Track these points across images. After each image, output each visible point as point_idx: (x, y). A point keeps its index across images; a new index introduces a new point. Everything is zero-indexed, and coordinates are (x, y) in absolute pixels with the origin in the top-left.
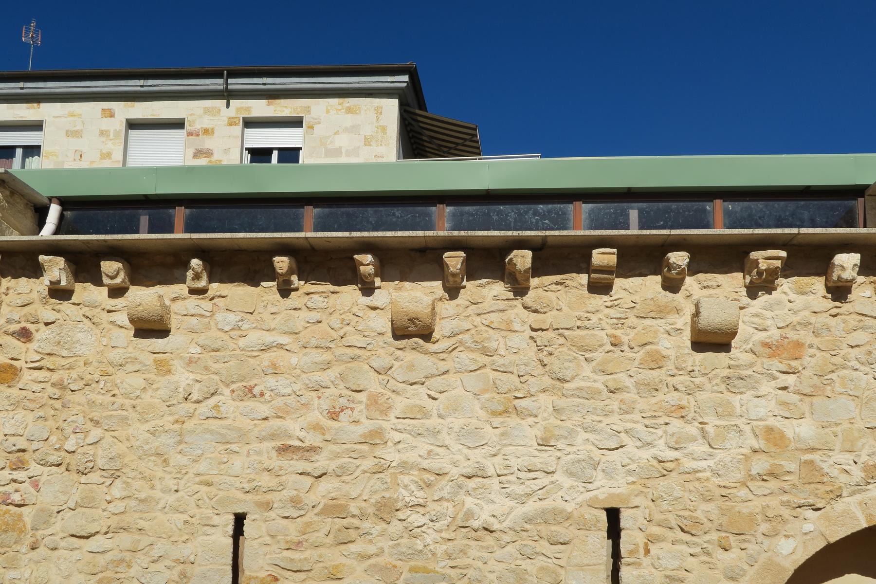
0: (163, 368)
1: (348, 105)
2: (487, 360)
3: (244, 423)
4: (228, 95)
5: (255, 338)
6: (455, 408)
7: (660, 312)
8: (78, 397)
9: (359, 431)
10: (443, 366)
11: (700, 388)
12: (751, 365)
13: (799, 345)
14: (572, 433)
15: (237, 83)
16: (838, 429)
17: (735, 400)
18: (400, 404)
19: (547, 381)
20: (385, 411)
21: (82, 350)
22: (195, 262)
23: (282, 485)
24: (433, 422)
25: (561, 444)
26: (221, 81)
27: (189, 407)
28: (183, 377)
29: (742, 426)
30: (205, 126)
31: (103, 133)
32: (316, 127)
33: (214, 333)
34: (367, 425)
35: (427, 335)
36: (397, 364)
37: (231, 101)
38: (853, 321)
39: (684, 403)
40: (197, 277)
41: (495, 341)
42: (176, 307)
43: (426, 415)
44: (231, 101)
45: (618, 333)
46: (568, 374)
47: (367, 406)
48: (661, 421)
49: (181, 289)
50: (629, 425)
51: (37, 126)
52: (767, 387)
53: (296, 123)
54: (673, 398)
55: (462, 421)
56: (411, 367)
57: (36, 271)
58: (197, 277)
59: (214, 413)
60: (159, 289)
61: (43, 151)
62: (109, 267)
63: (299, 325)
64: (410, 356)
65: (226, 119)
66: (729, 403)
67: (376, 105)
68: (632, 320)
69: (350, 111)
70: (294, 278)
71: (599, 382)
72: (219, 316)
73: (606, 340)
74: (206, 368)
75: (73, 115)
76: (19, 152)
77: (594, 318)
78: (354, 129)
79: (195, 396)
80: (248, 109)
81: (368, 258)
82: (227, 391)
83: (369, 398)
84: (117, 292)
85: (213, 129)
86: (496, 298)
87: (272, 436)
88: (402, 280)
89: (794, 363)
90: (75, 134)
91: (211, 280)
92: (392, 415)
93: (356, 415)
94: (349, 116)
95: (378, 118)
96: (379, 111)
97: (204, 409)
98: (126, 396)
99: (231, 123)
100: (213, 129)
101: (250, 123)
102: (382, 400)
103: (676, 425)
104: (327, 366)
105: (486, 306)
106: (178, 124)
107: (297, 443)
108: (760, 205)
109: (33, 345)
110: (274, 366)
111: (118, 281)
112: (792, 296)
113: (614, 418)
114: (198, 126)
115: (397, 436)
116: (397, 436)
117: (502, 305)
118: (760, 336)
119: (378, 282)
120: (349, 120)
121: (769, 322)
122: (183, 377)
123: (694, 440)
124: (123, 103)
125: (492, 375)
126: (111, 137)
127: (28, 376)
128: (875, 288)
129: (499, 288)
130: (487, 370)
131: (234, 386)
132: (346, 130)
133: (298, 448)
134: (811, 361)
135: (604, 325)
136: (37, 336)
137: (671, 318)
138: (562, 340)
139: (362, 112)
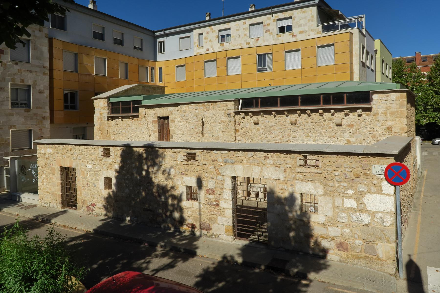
0: (259, 129)
2: (305, 128)
3: (270, 138)
4: (273, 13)
5: (271, 124)
6: (300, 136)
7: (331, 119)
8: (247, 134)
9: (287, 139)
10: (298, 129)
11: (337, 133)
12: (345, 129)
13: (353, 125)
14: (318, 140)
15: (274, 10)
16: (359, 140)
17: (343, 135)
18: (292, 135)
19: (314, 131)
20: (290, 136)
21: (247, 127)
22: (262, 113)
24: (297, 138)
25: (316, 142)
26: (270, 10)
27: (263, 136)
28: (261, 131)
29: (344, 139)
30: (268, 23)
31: (244, 29)
33: (265, 124)
34: (288, 139)
35: (296, 124)
36: (292, 128)
38: (362, 120)
39: (335, 135)
40: (262, 115)
41: (306, 124)
42: (260, 119)
43: (296, 137)
45: (325, 123)
46: (317, 130)
47: (288, 135)
48: (331, 138)
49: (260, 116)
50: (326, 139)
51: (229, 29)
52: (348, 132)
53: (290, 18)
54: (333, 134)
55: (301, 138)
56: (294, 129)
57: (240, 115)
58: (262, 115)
59: (266, 137)
60: (257, 116)
61: (231, 35)
62: (250, 114)
63: (277, 122)
64: (294, 127)
65: (272, 20)
66: (341, 135)
67: (310, 9)
68: (327, 121)
69: (304, 12)
70: (276, 115)
71: (322, 131)
72: (266, 121)
73: (323, 124)
74: (264, 129)
75: (237, 25)
76: (226, 36)
77: (321, 120)
78: (305, 18)
79: (263, 134)
80: (278, 16)
81: (286, 112)
82: (268, 133)
83: (288, 134)
84: (251, 117)
85: (270, 23)
86: (306, 117)
87: (274, 141)
88: (292, 114)
89: (352, 128)
90: (238, 30)
91: (264, 115)
92: (291, 137)
93: (286, 137)
94: (304, 14)
95: (311, 13)
96: (311, 11)
97: (265, 136)
98: (254, 134)
99: (274, 21)
100: (270, 23)
101: (278, 20)
102: (290, 135)
103: (334, 139)
104: (281, 129)
105: (304, 118)
106: (261, 23)
107: (278, 142)
109: (241, 126)
110: (274, 129)
111: (251, 116)
112: (352, 116)
113: (324, 138)
114: (266, 23)
115: (292, 141)
116: (292, 141)
117: (307, 118)
118: (347, 123)
119: (288, 115)
120: (303, 15)
121: (348, 121)
122: (261, 131)
123: (336, 141)
124: (248, 20)
125: (306, 130)
127: (240, 131)
128: (437, 65)
129: (306, 115)
130: (305, 129)
131: (269, 132)
133: (278, 142)
134: (355, 128)
135: (322, 122)
136: (241, 124)
137: (333, 121)
138: (316, 124)
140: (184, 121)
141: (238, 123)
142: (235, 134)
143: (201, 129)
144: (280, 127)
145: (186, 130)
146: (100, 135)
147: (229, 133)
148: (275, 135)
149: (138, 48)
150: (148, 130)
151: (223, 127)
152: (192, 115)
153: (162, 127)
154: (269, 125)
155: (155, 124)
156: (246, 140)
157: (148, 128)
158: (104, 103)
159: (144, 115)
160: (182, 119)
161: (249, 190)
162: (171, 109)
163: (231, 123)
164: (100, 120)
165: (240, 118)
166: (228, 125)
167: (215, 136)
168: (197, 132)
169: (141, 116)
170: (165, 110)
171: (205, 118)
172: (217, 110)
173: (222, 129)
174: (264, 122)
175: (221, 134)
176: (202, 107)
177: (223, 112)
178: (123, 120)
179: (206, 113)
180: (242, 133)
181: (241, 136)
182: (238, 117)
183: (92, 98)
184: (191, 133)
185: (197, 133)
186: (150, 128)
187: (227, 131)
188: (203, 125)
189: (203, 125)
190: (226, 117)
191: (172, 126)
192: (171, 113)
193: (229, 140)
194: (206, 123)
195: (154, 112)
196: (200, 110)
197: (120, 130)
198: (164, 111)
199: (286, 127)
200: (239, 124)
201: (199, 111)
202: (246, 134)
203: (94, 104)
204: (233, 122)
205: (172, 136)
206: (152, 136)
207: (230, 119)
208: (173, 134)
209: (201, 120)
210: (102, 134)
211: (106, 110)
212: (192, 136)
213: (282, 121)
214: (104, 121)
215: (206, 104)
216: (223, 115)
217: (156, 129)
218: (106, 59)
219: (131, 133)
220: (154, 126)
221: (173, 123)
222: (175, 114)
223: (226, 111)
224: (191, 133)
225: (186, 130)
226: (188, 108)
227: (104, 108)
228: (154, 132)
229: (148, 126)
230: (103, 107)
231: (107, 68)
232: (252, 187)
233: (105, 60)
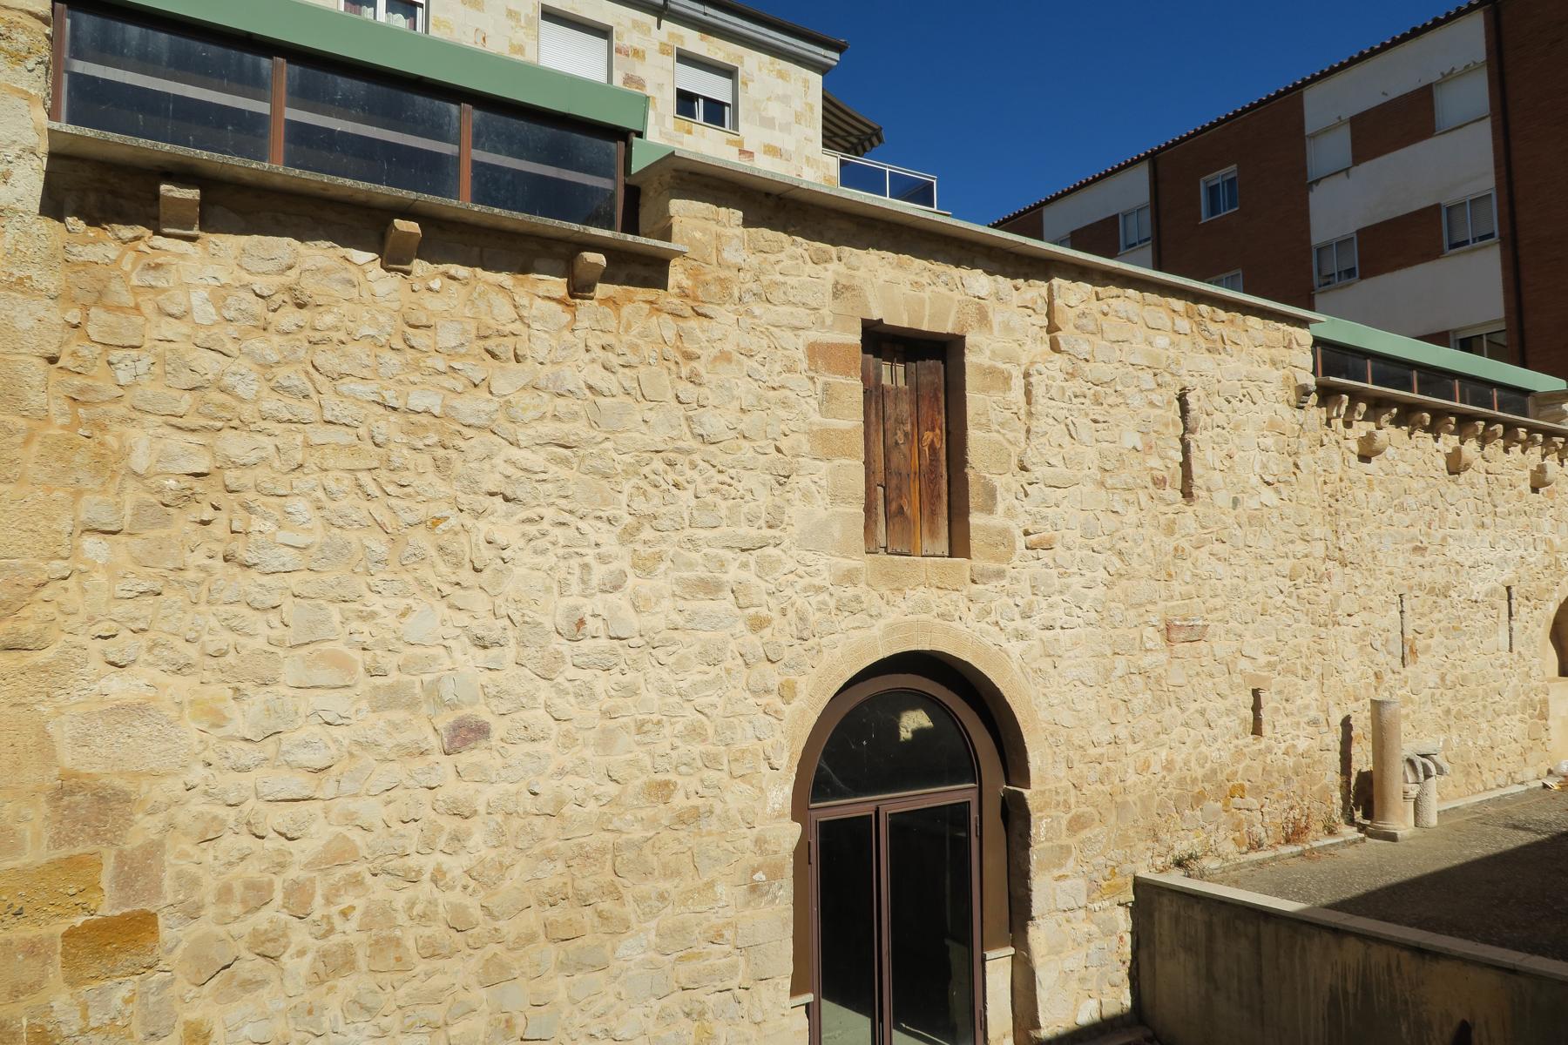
1: (778, 67)
23: (503, 559)
32: (750, 84)
37: (663, 21)
44: (663, 21)
51: (729, 72)
69: (781, 75)
78: (785, 99)
80: (680, 38)
101: (685, 58)
108: (163, 38)
126: (523, 23)
132: (778, 98)
139: (792, 81)
155: (841, 379)
160: (1073, 375)
162: (979, 282)
169: (695, 274)
171: (1199, 391)
176: (1184, 324)
184: (1125, 476)
192: (983, 318)
205: (991, 494)
206: (800, 481)
208: (998, 481)
219: (549, 429)
220: (828, 396)
221: (997, 396)
222: (1007, 328)
224: (1125, 476)
228: (826, 445)
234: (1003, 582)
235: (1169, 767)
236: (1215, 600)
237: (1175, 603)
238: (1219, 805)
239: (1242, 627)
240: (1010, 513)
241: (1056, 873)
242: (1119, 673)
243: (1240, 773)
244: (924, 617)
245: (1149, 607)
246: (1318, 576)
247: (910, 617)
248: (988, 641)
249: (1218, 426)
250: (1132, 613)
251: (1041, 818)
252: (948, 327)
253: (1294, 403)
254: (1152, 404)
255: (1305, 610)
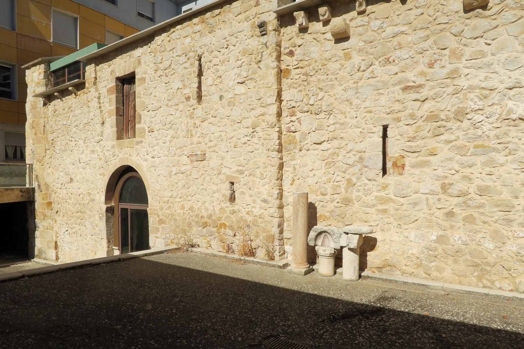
3: (386, 78)
5: (390, 30)
8: (313, 79)
9: (445, 71)
10: (494, 23)
21: (313, 55)
24: (489, 58)
27: (360, 74)
34: (450, 68)
42: (352, 24)
49: (354, 14)
55: (506, 55)
59: (372, 75)
63: (412, 18)
72: (372, 24)
74: (367, 52)
79: (362, 68)
92: (463, 59)
93: (443, 63)
97: (367, 74)
98: (333, 74)
107: (412, 84)
109: (295, 58)
110: (399, 44)
115: (466, 71)
116: (466, 71)
131: (380, 59)
136: (296, 53)
140: (162, 73)
141: (287, 51)
142: (279, 83)
143: (196, 85)
144: (422, 34)
145: (166, 95)
146: (34, 136)
147: (262, 81)
148: (402, 63)
149: (144, 16)
150: (99, 111)
151: (246, 67)
152: (177, 54)
153: (126, 103)
154: (383, 35)
156: (311, 94)
157: (100, 107)
158: (40, 73)
159: (93, 80)
161: (312, 244)
163: (268, 51)
164: (34, 107)
165: (294, 33)
166: (259, 59)
167: (228, 96)
168: (187, 96)
170: (128, 58)
171: (206, 54)
172: (234, 22)
173: (245, 74)
174: (367, 31)
175: (241, 89)
177: (246, 24)
178: (64, 99)
179: (208, 39)
180: (297, 77)
181: (296, 86)
182: (292, 30)
183: (23, 67)
185: (188, 99)
186: (104, 106)
187: (255, 76)
188: (200, 74)
189: (200, 74)
190: (255, 37)
191: (140, 93)
193: (261, 100)
194: (206, 67)
195: (110, 69)
196: (193, 36)
197: (60, 122)
198: (126, 61)
199: (444, 26)
200: (291, 53)
201: (192, 39)
202: (310, 79)
203: (26, 78)
204: (272, 45)
207: (264, 39)
209: (197, 63)
210: (36, 134)
211: (41, 86)
212: (176, 107)
213: (431, 11)
214: (39, 109)
215: (208, 14)
216: (247, 34)
217: (113, 107)
218: (78, 18)
223: (256, 19)
224: (175, 101)
225: (166, 95)
226: (168, 39)
227: (39, 83)
229: (100, 103)
230: (38, 81)
231: (80, 34)
232: (323, 235)
233: (76, 19)
234: (142, 144)
235: (191, 209)
236: (210, 143)
237: (194, 146)
238: (215, 229)
239: (225, 154)
240: (145, 123)
241: (155, 235)
242: (174, 172)
243: (223, 218)
244: (126, 156)
245: (185, 148)
246: (270, 124)
247: (124, 156)
248: (138, 162)
249: (215, 65)
250: (179, 151)
251: (151, 217)
252: (132, 71)
253: (259, 34)
254: (185, 68)
255: (261, 143)
